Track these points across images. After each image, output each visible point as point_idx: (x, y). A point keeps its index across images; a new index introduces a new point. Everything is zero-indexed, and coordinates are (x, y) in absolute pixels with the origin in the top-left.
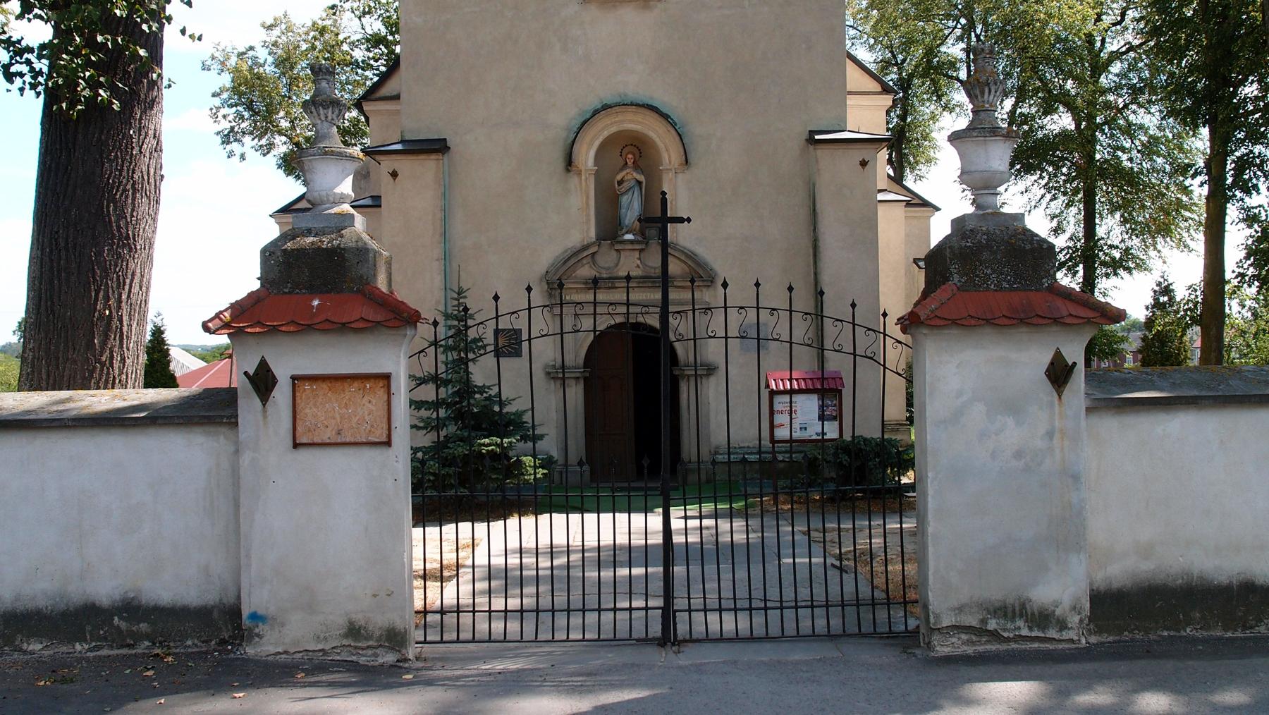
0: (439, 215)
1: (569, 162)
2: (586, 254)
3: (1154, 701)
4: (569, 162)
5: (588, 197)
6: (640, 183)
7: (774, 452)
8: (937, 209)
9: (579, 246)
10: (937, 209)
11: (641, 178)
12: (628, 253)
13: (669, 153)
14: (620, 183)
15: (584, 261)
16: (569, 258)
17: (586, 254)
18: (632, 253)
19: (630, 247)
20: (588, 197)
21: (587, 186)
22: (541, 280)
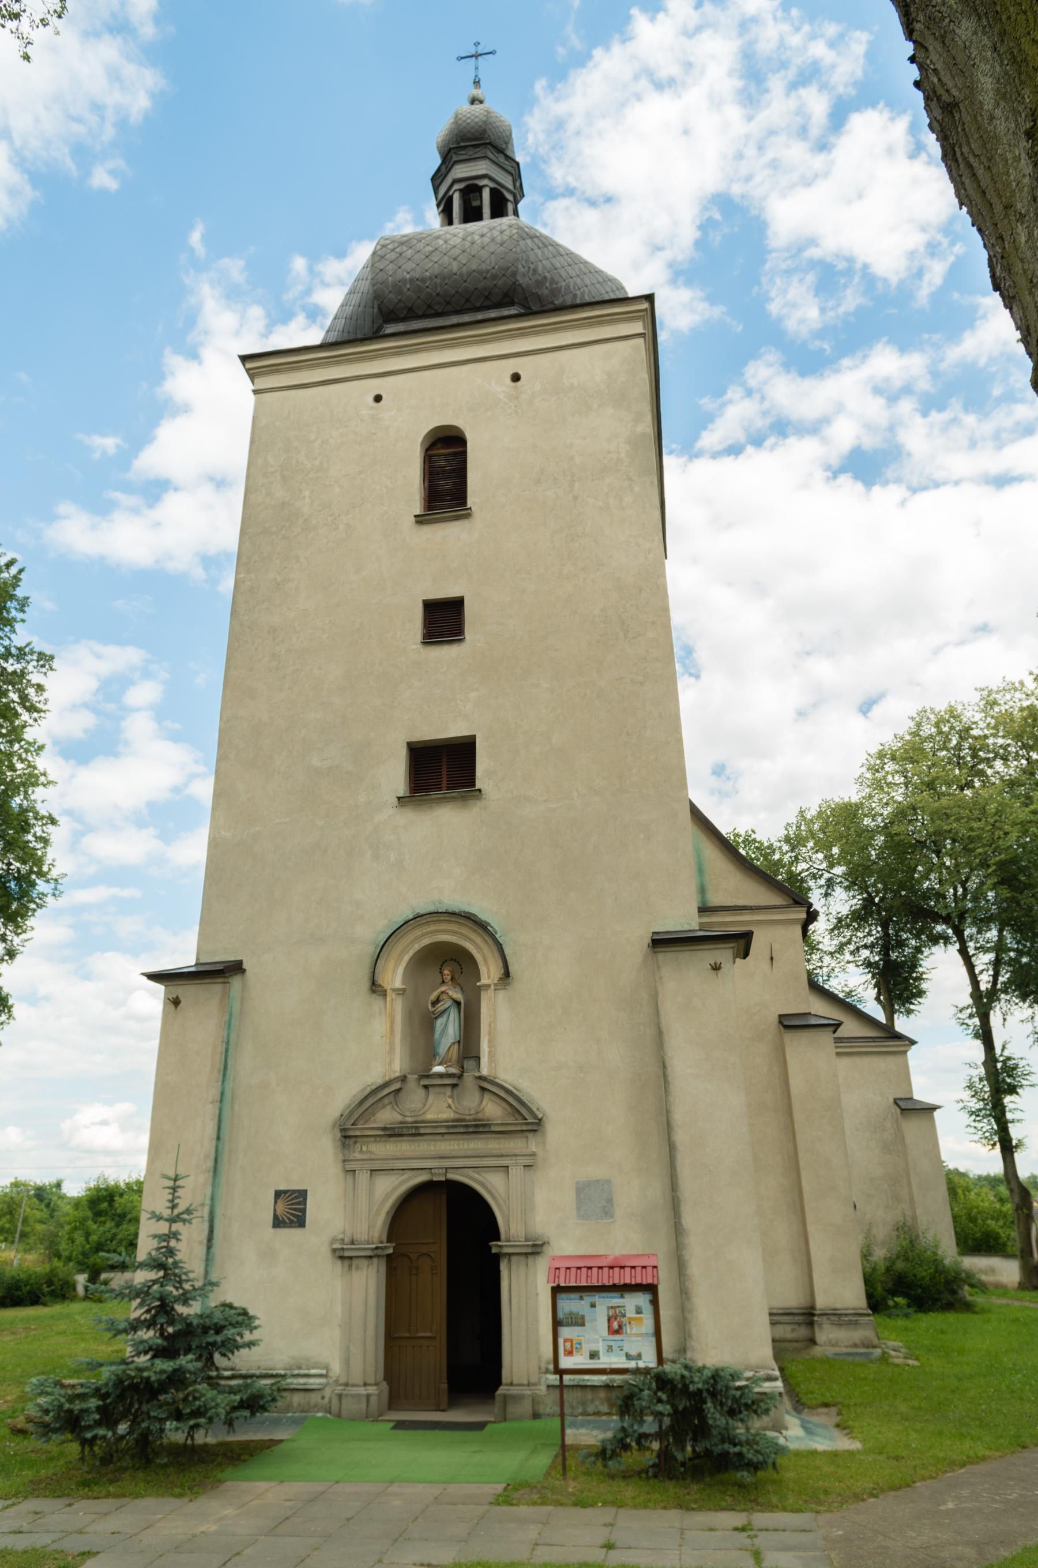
0: (221, 1048)
1: (375, 987)
2: (386, 1091)
3: (1035, 1204)
4: (375, 987)
5: (392, 1022)
6: (458, 1003)
7: (887, 865)
8: (913, 1042)
9: (380, 1081)
10: (913, 1042)
11: (458, 996)
12: (437, 1090)
13: (489, 972)
14: (435, 1003)
15: (386, 1101)
16: (366, 1098)
17: (386, 1091)
18: (442, 1090)
19: (439, 1082)
20: (392, 1022)
21: (393, 1009)
22: (334, 1126)
